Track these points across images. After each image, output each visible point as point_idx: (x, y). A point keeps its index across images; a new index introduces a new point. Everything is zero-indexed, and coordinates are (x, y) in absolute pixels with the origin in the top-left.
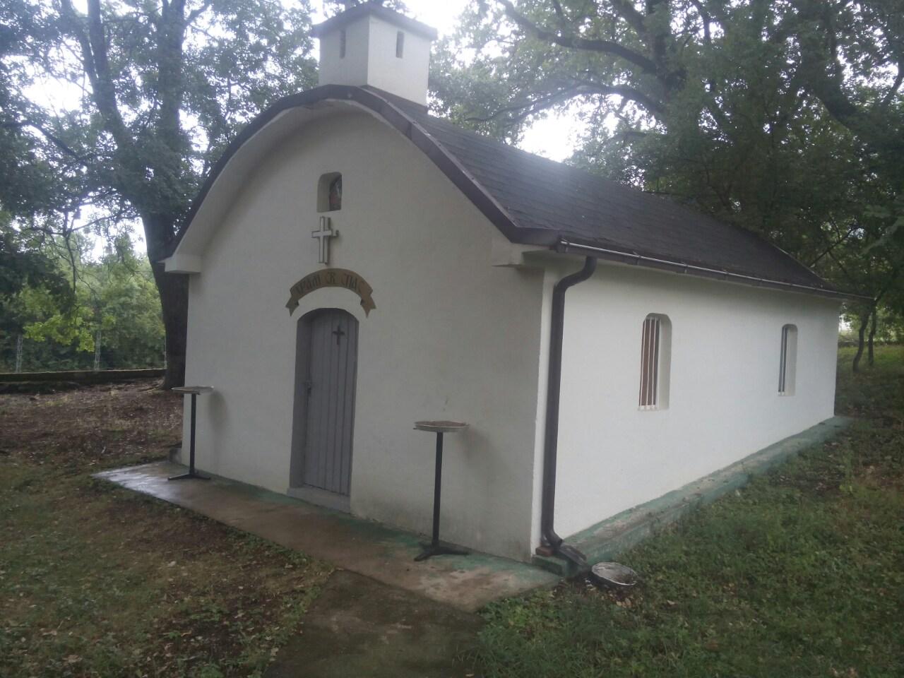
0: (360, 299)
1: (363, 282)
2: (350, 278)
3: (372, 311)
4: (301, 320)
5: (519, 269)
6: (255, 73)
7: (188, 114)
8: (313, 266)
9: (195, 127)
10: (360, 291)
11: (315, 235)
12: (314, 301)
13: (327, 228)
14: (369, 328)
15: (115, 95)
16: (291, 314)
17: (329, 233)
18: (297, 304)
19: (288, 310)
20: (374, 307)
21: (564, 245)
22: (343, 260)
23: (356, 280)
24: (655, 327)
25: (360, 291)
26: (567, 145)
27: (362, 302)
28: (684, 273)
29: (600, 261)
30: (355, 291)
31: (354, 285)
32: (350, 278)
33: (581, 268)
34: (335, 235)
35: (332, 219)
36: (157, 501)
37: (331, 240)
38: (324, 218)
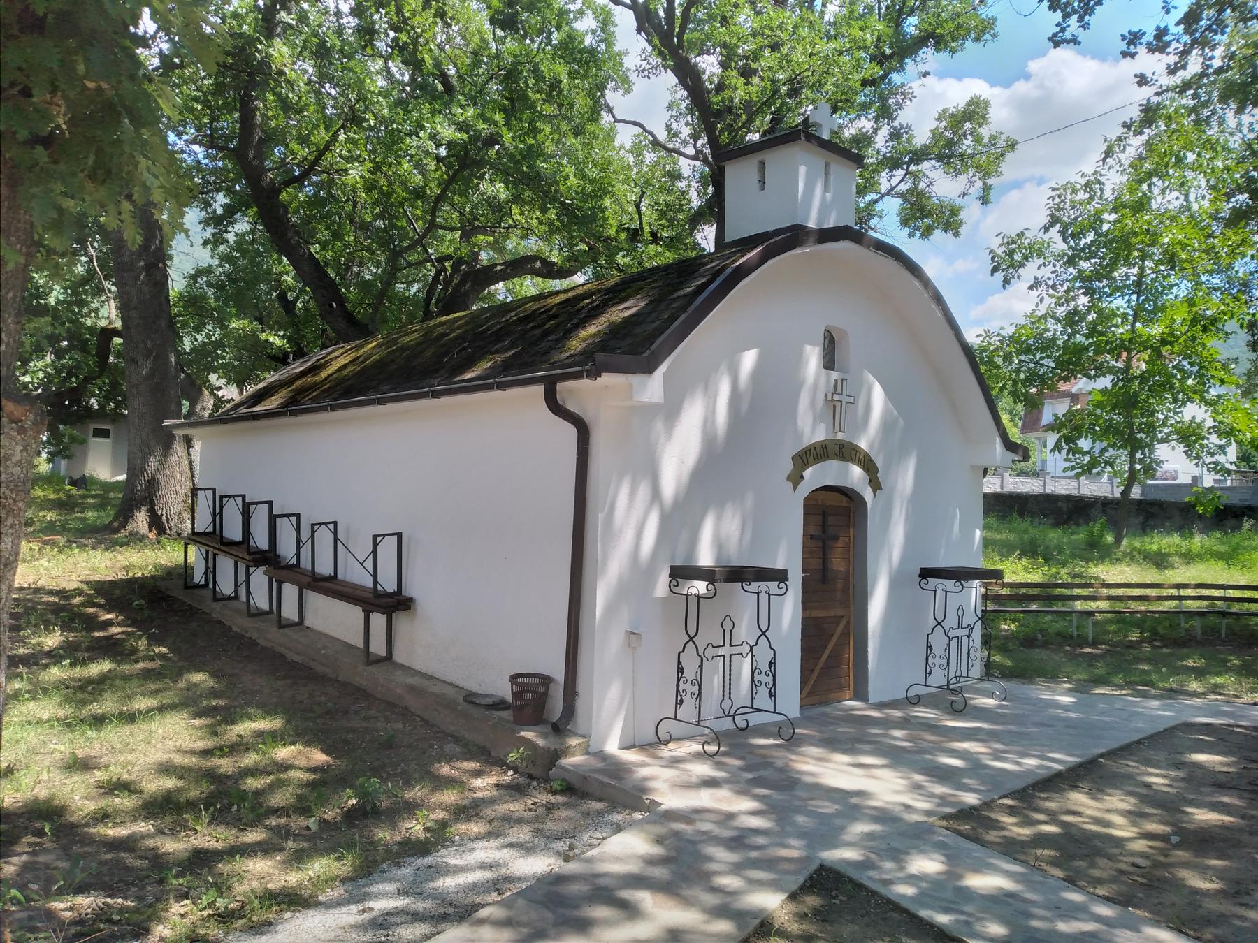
16: (795, 489)
18: (802, 477)
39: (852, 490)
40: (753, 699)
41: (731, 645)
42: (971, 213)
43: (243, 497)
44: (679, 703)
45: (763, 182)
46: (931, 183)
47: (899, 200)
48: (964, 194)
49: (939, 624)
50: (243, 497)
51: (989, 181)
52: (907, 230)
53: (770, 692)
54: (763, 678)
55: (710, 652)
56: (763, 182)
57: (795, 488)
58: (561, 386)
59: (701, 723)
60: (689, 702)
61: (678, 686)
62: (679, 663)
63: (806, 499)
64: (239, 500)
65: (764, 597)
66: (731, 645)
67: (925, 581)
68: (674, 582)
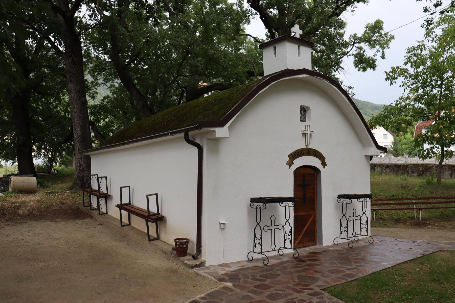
1: (322, 155)
6: (443, 30)
8: (302, 146)
9: (2, 204)
14: (324, 172)
15: (62, 115)
16: (290, 168)
18: (293, 163)
20: (326, 165)
22: (313, 146)
27: (322, 164)
30: (319, 158)
31: (318, 156)
36: (335, 84)
39: (314, 167)
40: (285, 244)
41: (274, 226)
42: (379, 62)
43: (97, 175)
44: (255, 246)
45: (275, 54)
46: (365, 51)
47: (353, 57)
48: (375, 55)
49: (364, 213)
50: (97, 175)
51: (384, 50)
52: (357, 69)
53: (366, 230)
54: (364, 226)
55: (266, 228)
56: (275, 54)
57: (290, 167)
58: (190, 133)
59: (262, 253)
60: (258, 246)
61: (254, 240)
62: (255, 233)
63: (294, 171)
64: (96, 176)
65: (287, 208)
66: (274, 226)
67: (339, 200)
68: (252, 204)
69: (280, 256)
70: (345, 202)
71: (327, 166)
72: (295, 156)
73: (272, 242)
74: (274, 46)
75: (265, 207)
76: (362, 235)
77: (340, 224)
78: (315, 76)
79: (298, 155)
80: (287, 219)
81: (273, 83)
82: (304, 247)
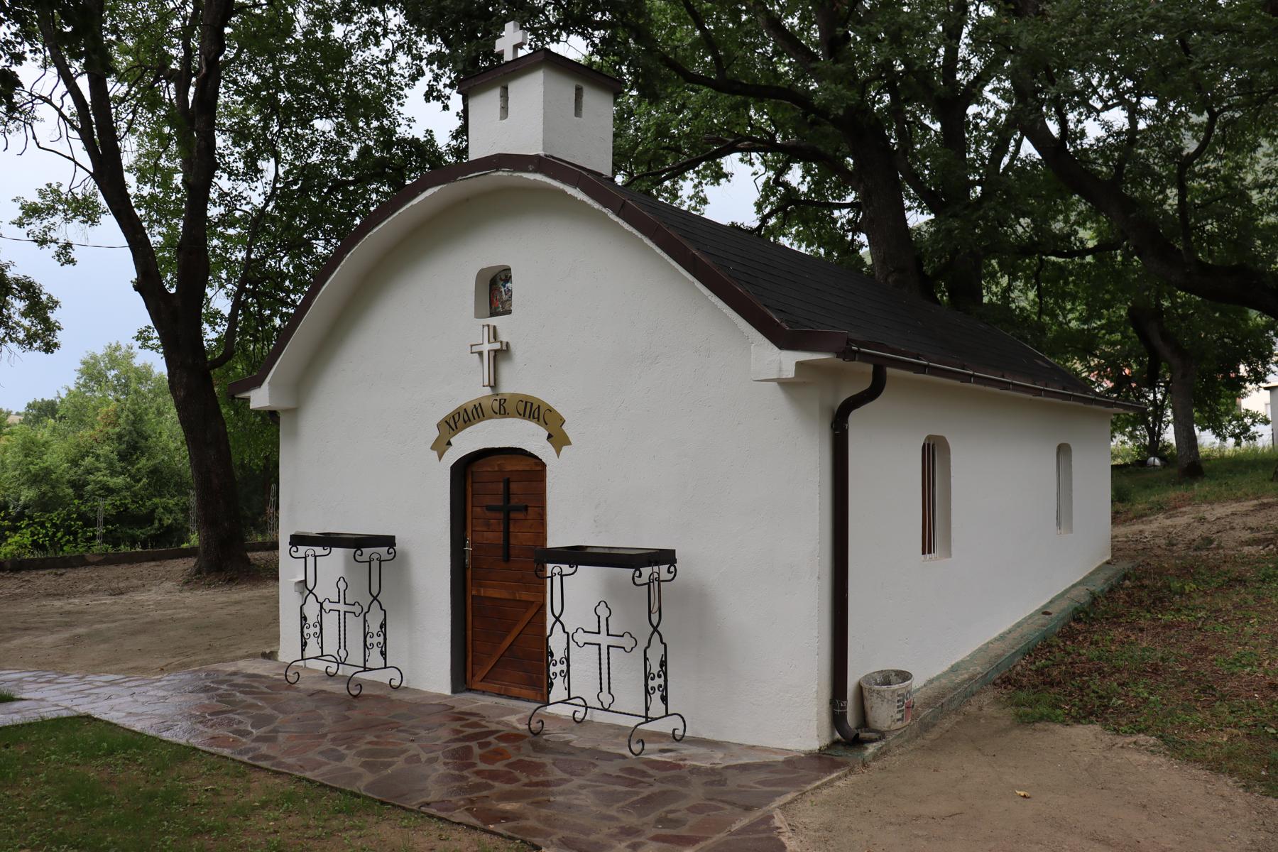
0: (546, 434)
1: (550, 410)
2: (529, 405)
3: (565, 449)
4: (453, 468)
5: (784, 384)
7: (743, 224)
8: (474, 389)
10: (547, 424)
11: (475, 349)
12: (468, 441)
13: (492, 339)
16: (558, 455)
17: (497, 346)
18: (449, 444)
19: (435, 454)
21: (854, 351)
22: (515, 382)
23: (539, 407)
24: (933, 453)
25: (547, 424)
26: (15, 200)
27: (550, 436)
28: (970, 382)
29: (890, 371)
31: (536, 416)
32: (529, 405)
33: (865, 385)
34: (504, 348)
35: (498, 329)
36: (531, 167)
37: (501, 354)
38: (488, 326)
61: (321, 629)
67: (294, 549)
69: (575, 724)
70: (310, 552)
71: (569, 443)
72: (455, 423)
73: (609, 678)
74: (580, 84)
75: (672, 575)
76: (371, 670)
77: (301, 618)
78: (460, 178)
79: (466, 418)
80: (557, 613)
81: (348, 256)
82: (499, 695)
